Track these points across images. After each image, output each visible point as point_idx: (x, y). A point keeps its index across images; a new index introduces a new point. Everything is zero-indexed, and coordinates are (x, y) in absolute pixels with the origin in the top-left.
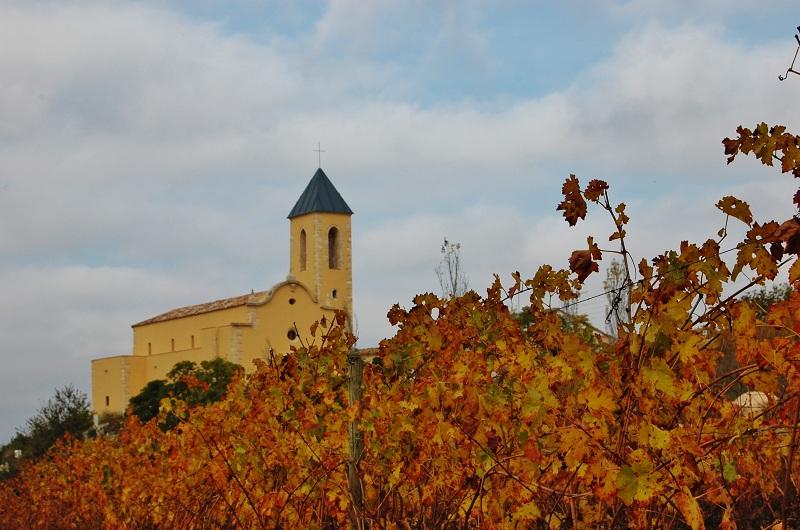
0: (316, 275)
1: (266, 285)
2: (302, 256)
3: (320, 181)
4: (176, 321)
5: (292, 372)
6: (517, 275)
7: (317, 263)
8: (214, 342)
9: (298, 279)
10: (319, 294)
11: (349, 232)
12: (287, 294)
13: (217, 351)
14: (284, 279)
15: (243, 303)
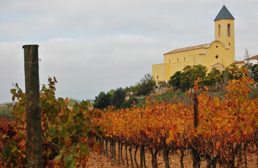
0: (224, 38)
1: (209, 42)
3: (224, 8)
4: (190, 51)
6: (57, 82)
7: (224, 35)
8: (193, 60)
9: (218, 40)
10: (225, 44)
12: (215, 44)
13: (194, 64)
14: (214, 40)
15: (201, 47)
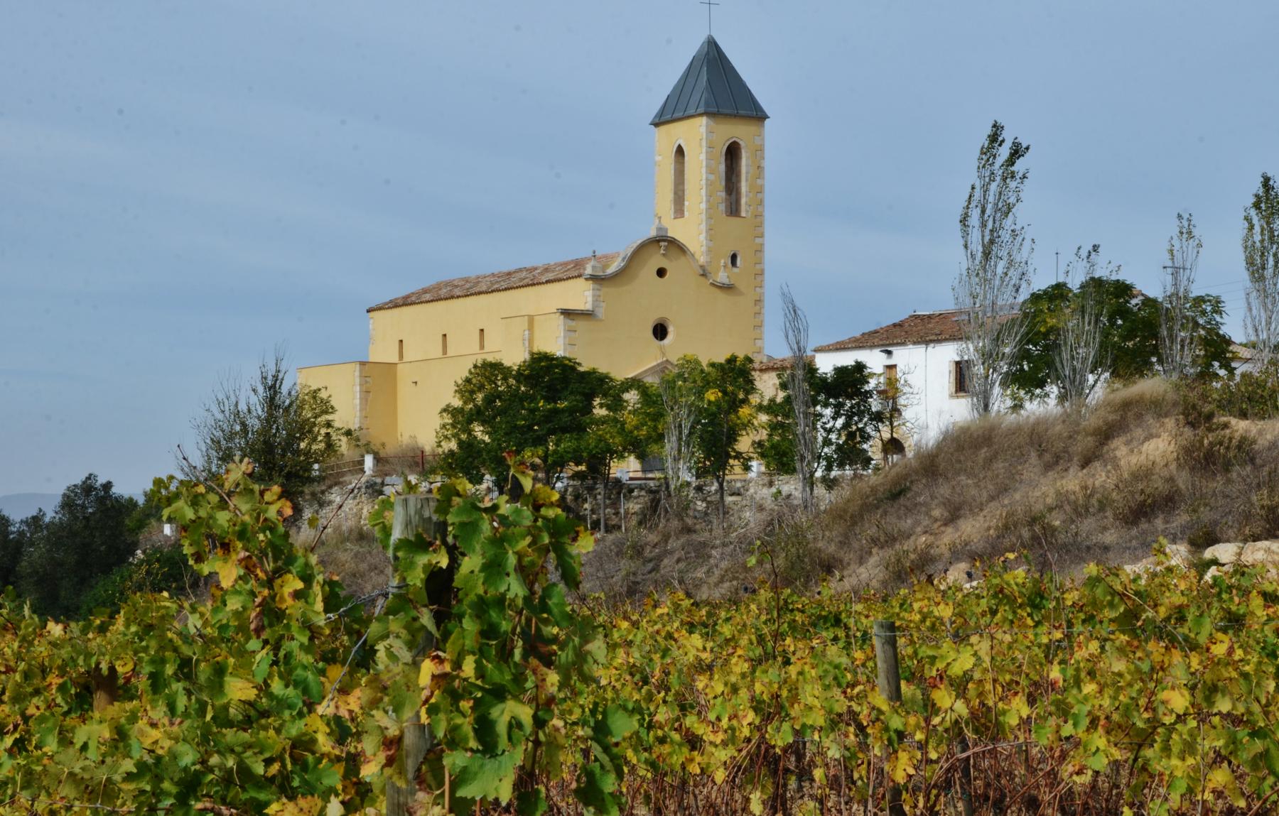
2: (675, 193)
5: (100, 698)
11: (759, 151)
